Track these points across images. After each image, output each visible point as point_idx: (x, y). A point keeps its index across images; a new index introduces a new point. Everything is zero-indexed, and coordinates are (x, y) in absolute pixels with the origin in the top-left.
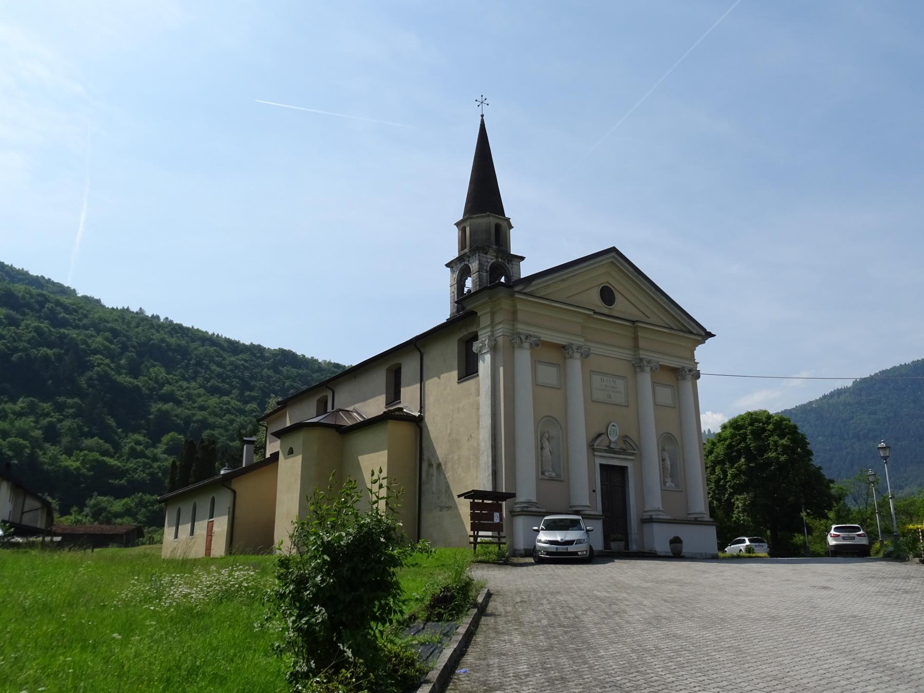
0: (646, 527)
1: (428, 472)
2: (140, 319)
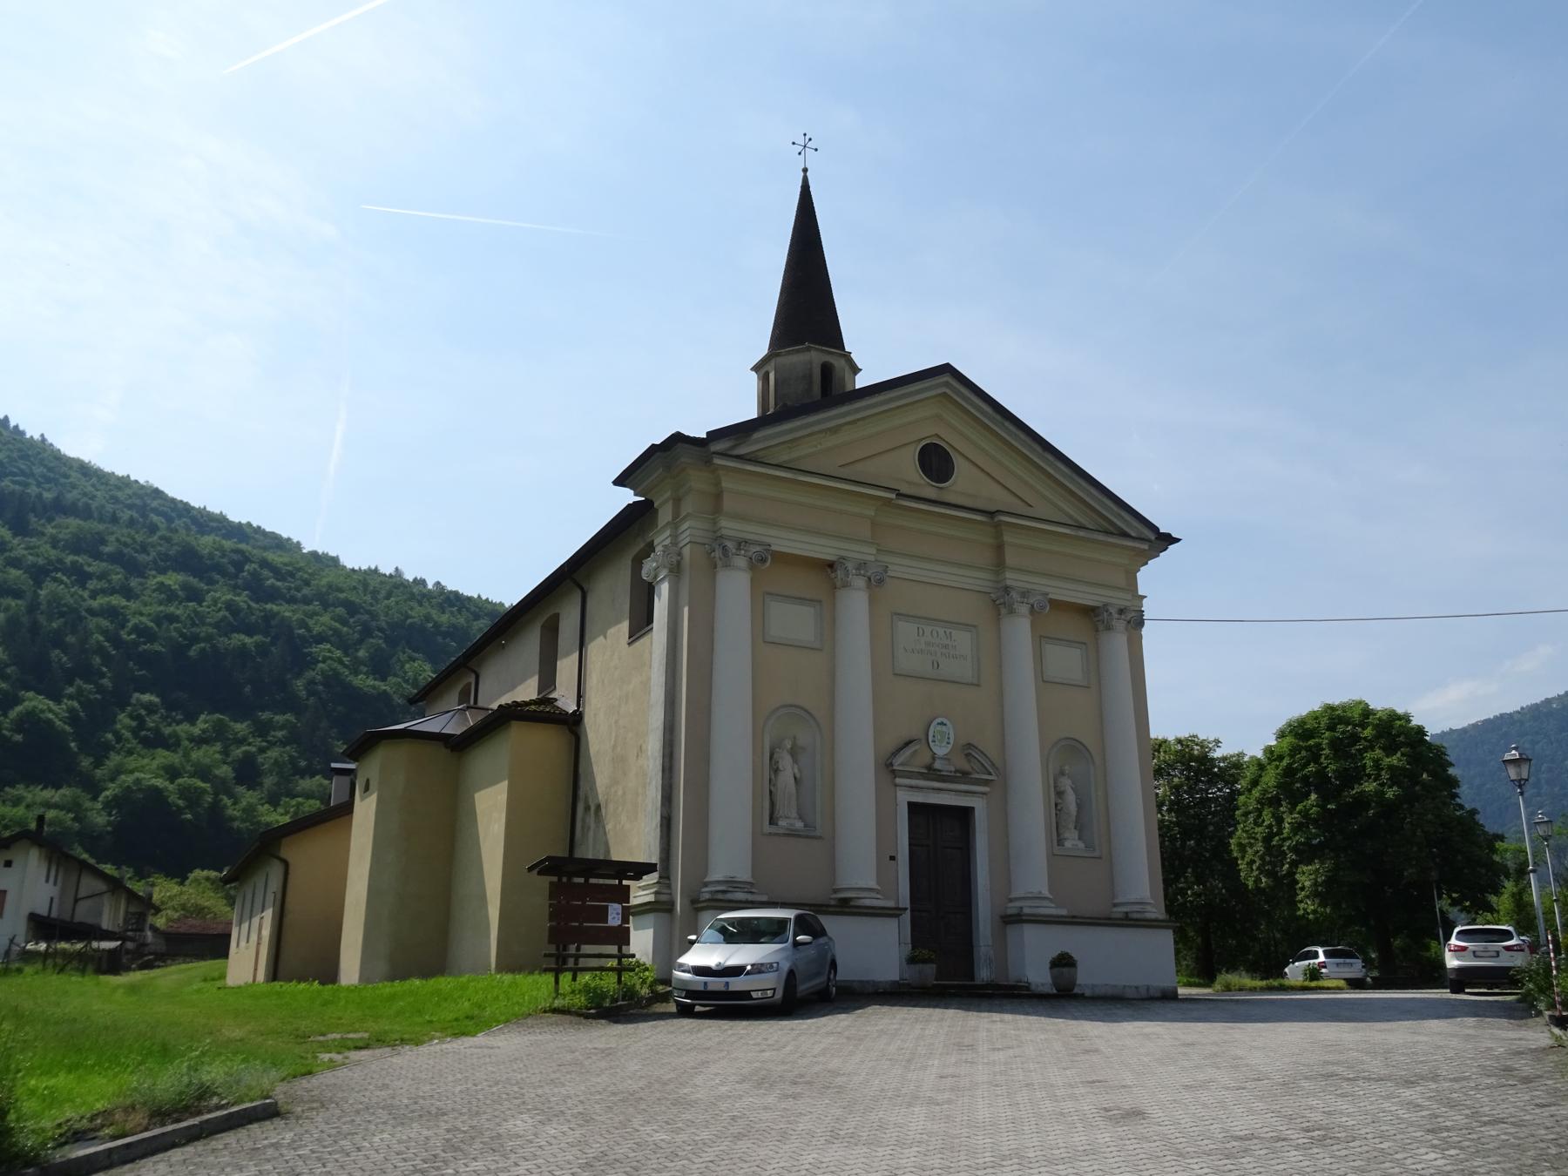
0: (1012, 931)
1: (583, 820)
2: (395, 584)
